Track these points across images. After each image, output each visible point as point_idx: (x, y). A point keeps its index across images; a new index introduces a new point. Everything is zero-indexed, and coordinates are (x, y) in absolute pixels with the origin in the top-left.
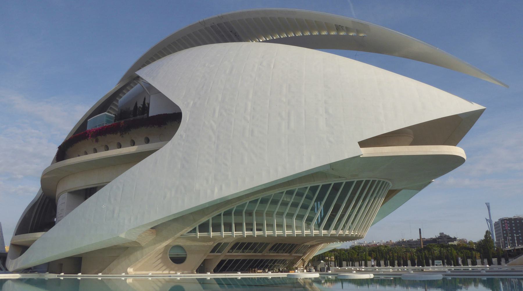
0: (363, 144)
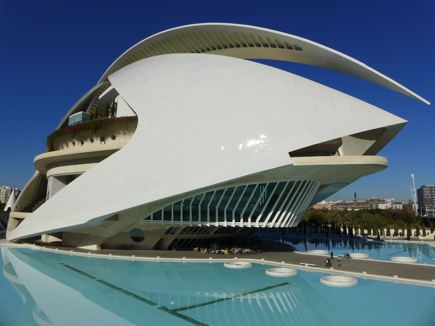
0: (293, 154)
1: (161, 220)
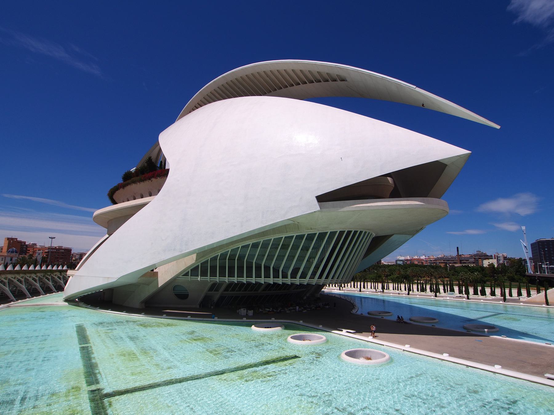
0: (321, 199)
1: (261, 277)
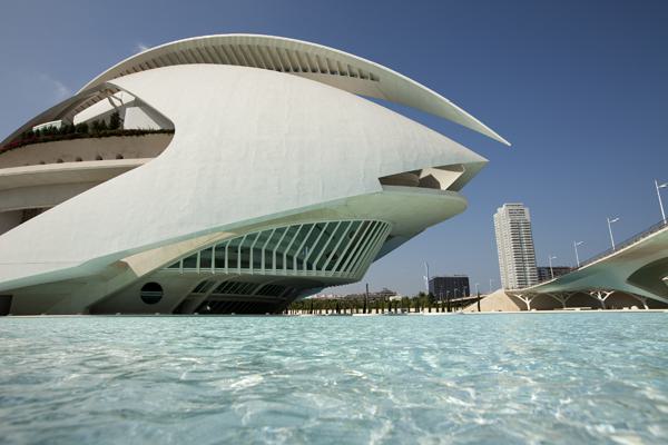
0: (385, 181)
